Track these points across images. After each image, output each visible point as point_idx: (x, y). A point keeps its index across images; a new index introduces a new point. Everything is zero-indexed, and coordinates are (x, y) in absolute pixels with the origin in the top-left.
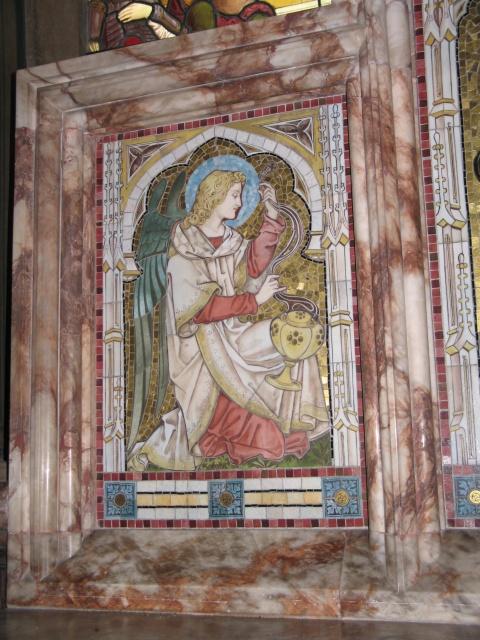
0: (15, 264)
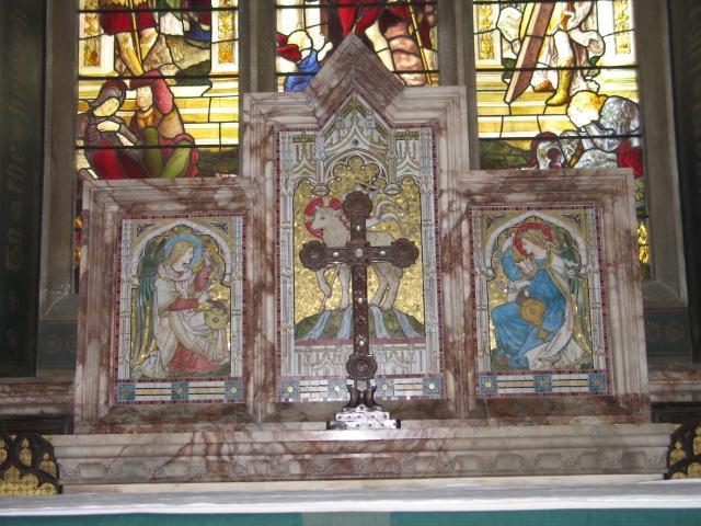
0: (81, 276)
